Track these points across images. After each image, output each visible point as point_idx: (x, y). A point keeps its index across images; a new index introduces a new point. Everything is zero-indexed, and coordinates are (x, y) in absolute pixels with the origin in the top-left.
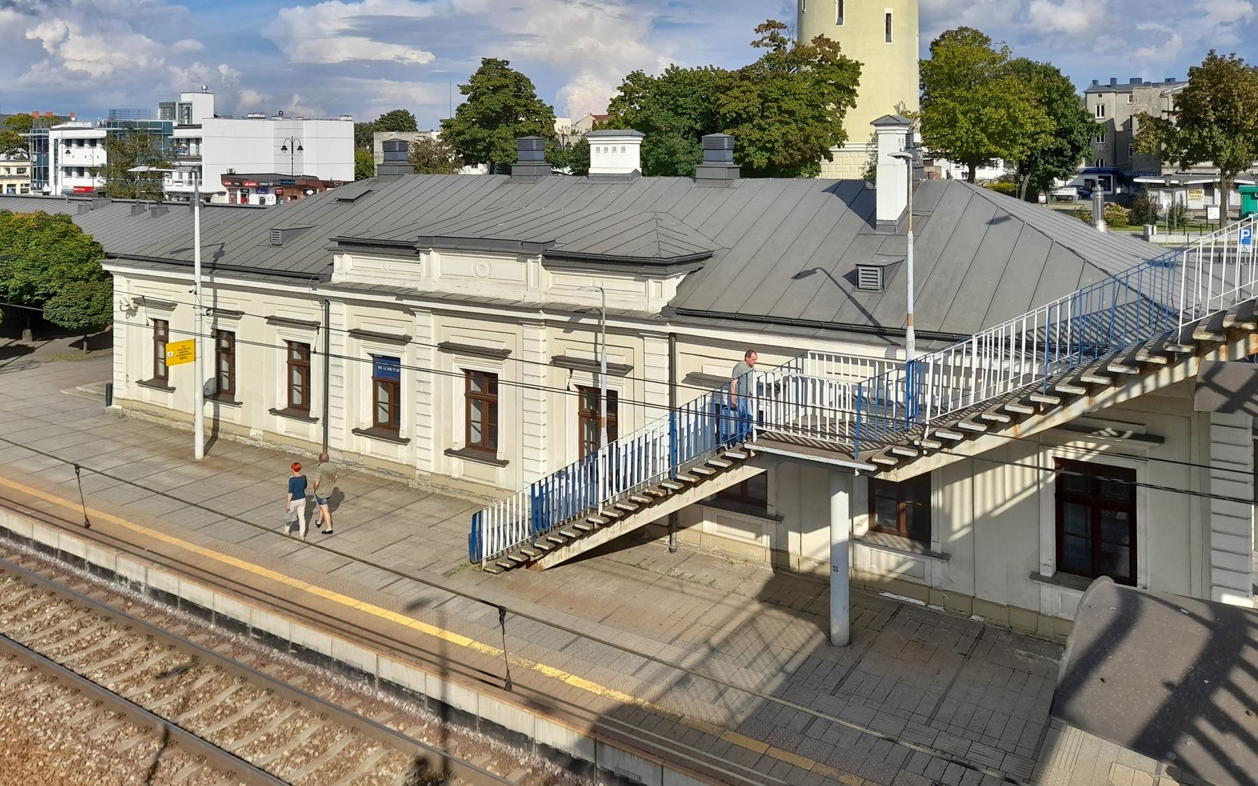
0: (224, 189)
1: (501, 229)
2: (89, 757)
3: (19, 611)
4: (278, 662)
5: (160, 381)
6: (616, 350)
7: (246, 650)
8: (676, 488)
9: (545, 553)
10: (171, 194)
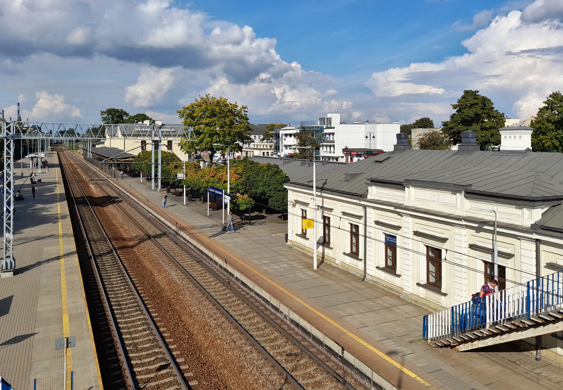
0: (343, 155)
1: (448, 178)
2: (260, 379)
3: (247, 317)
4: (333, 362)
5: (303, 235)
6: (504, 244)
7: (322, 353)
8: (530, 324)
9: (460, 343)
10: (323, 157)
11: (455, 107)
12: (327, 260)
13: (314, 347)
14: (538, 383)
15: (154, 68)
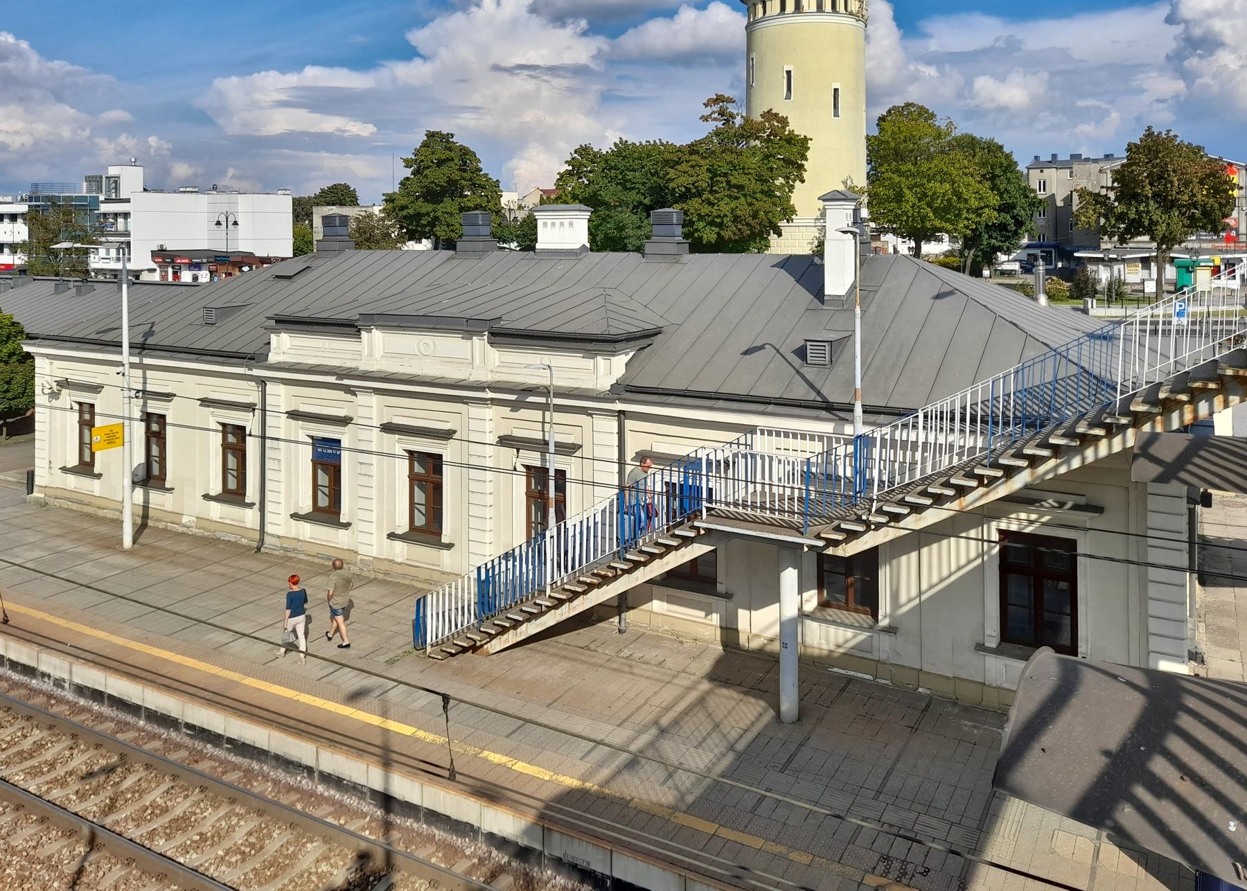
0: (154, 266)
1: (446, 306)
2: (9, 864)
4: (212, 758)
5: (86, 468)
6: (564, 428)
7: (178, 746)
8: (625, 567)
9: (492, 637)
10: (97, 271)
11: (408, 163)
12: (158, 520)
13: (155, 737)
14: (632, 673)
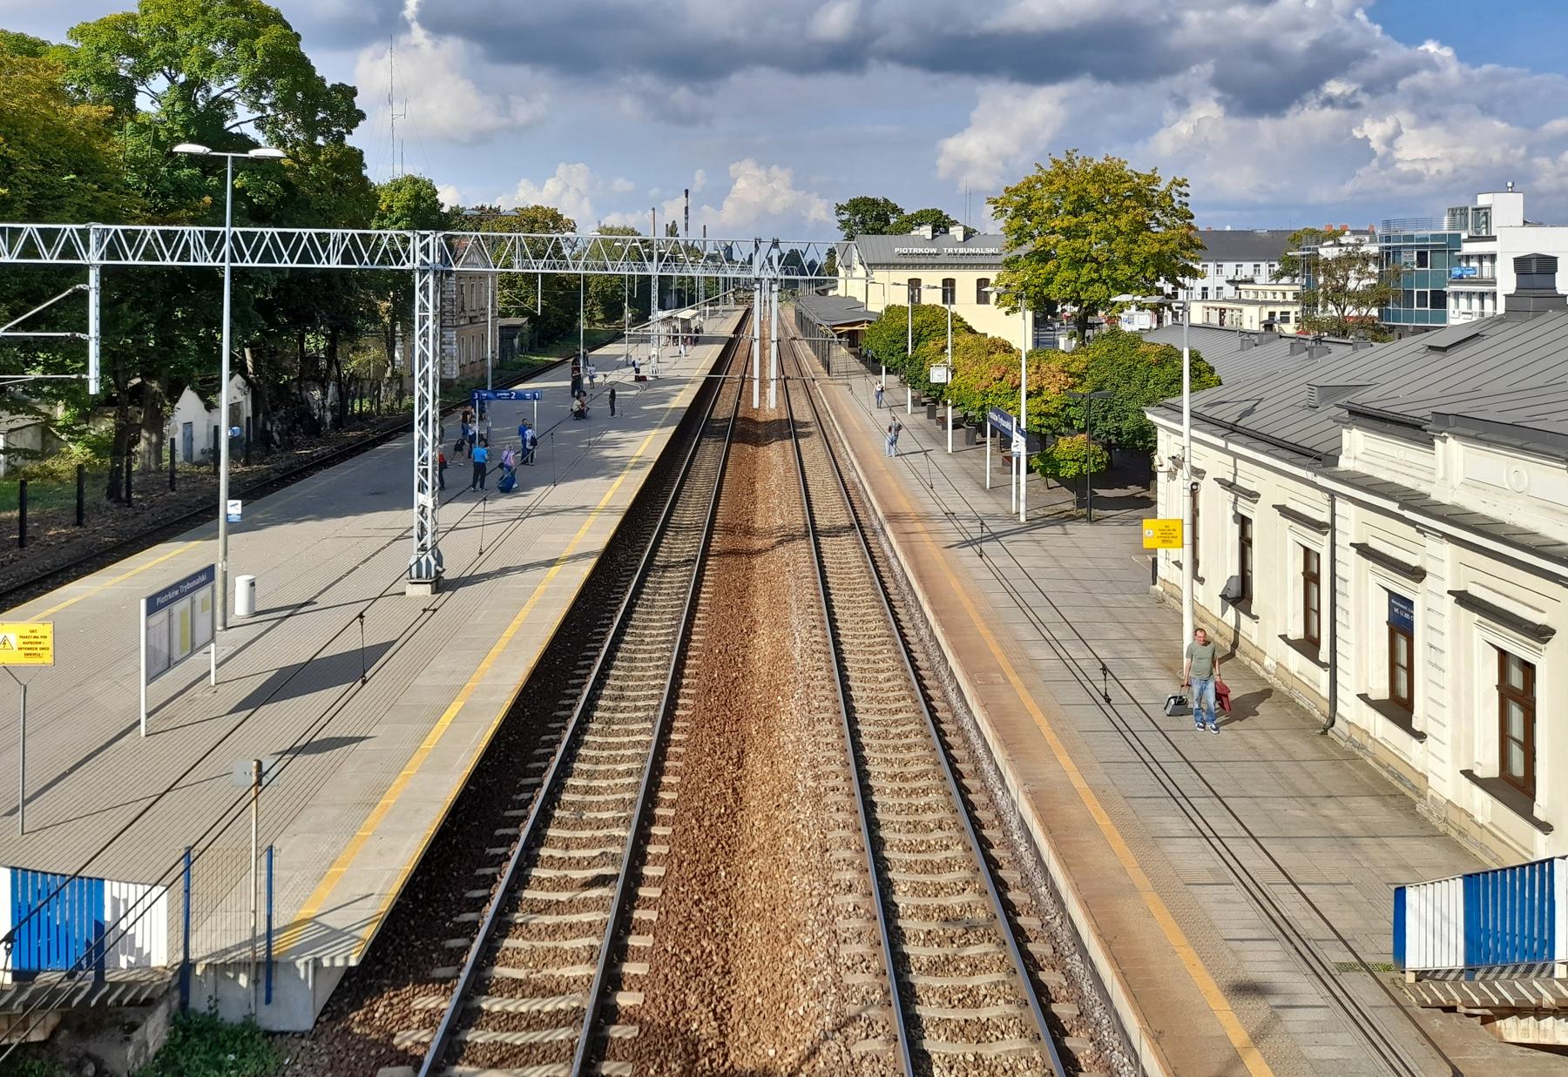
3: (907, 786)
15: (1017, 87)
